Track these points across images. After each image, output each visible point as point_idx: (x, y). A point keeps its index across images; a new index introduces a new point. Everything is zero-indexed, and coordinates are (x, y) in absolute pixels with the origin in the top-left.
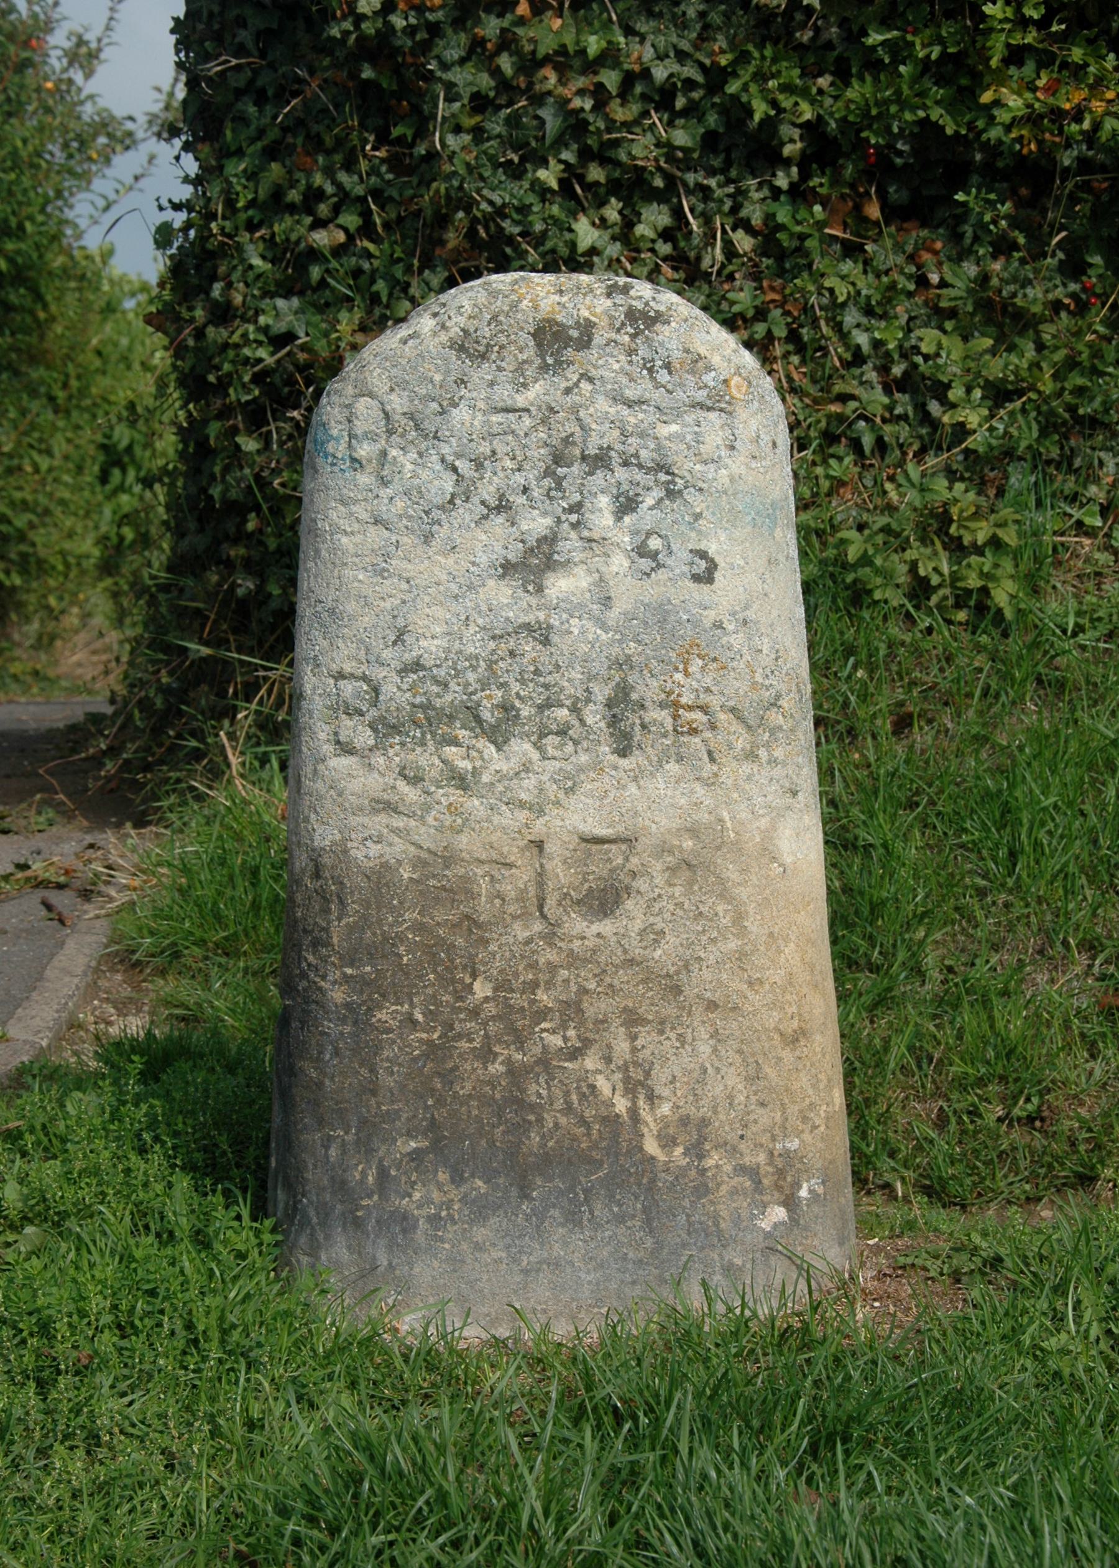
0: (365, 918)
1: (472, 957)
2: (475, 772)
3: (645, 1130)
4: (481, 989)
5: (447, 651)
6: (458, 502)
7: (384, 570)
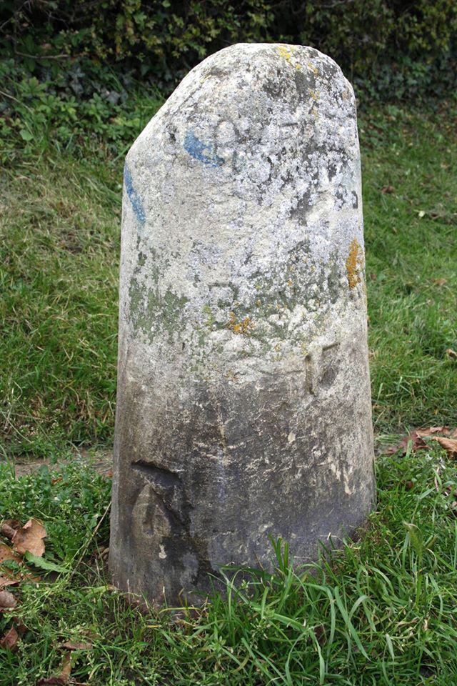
0: (238, 417)
1: (287, 423)
2: (286, 326)
3: (345, 482)
4: (291, 438)
5: (271, 263)
6: (272, 179)
7: (240, 222)
